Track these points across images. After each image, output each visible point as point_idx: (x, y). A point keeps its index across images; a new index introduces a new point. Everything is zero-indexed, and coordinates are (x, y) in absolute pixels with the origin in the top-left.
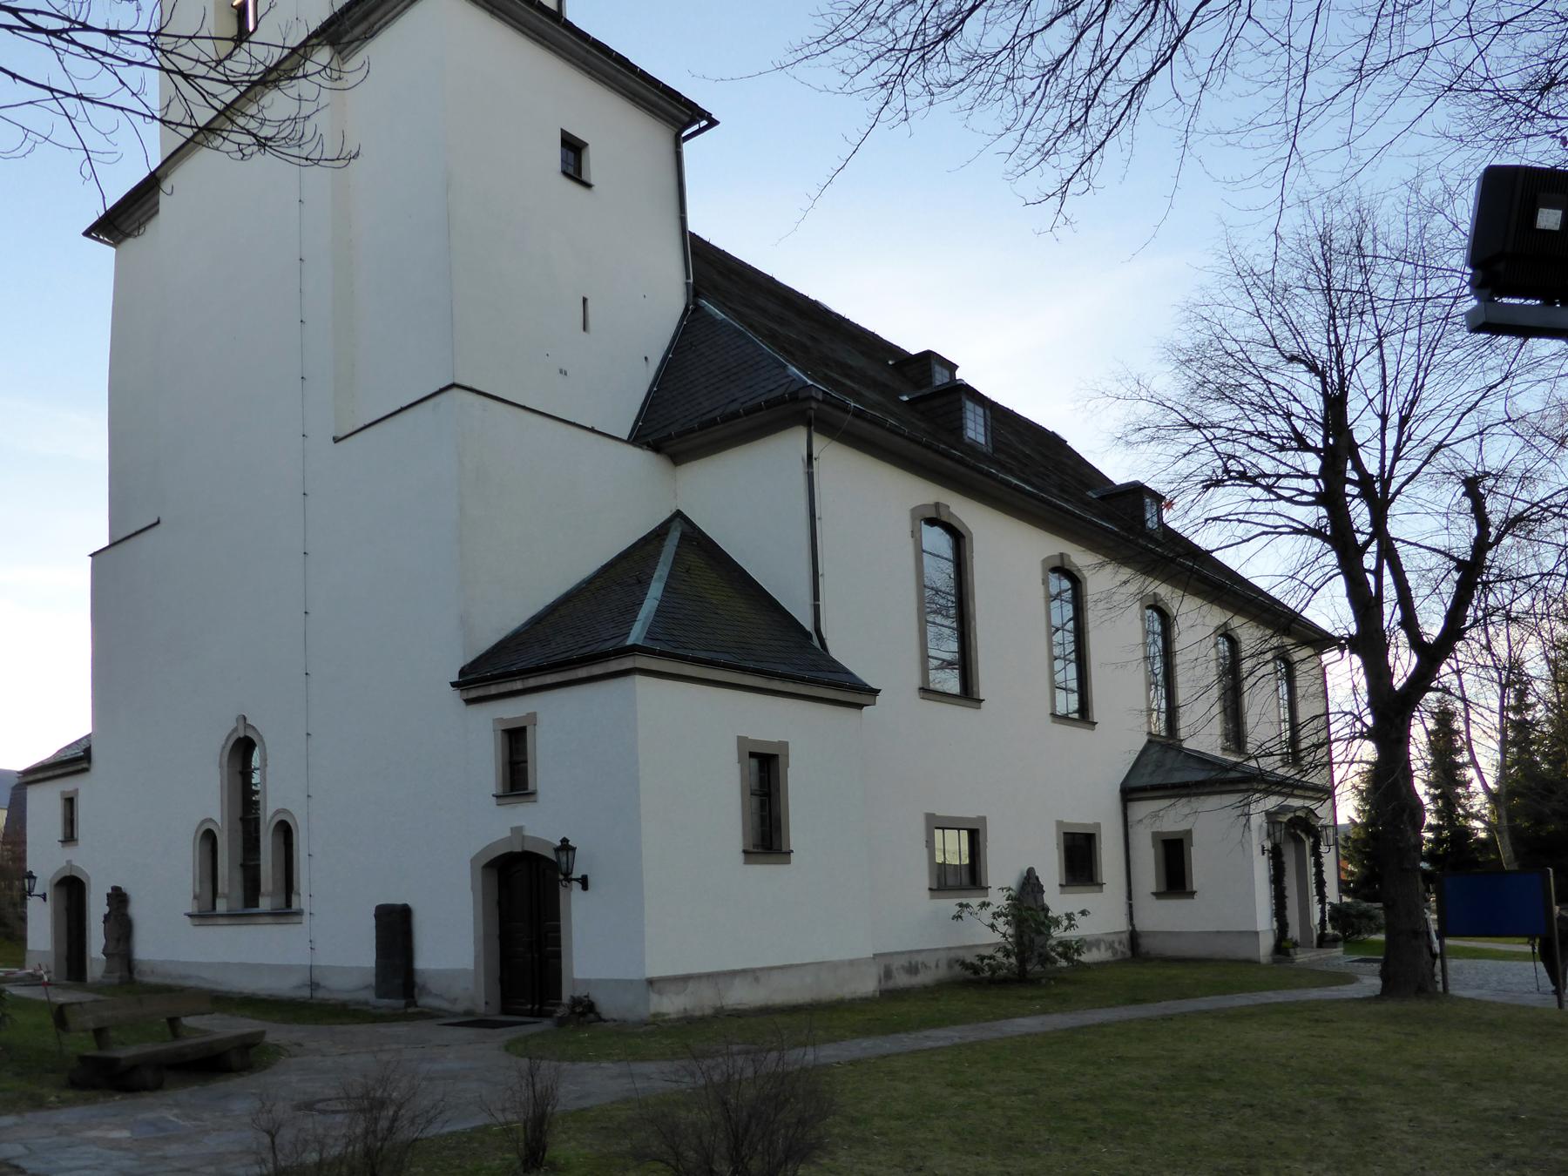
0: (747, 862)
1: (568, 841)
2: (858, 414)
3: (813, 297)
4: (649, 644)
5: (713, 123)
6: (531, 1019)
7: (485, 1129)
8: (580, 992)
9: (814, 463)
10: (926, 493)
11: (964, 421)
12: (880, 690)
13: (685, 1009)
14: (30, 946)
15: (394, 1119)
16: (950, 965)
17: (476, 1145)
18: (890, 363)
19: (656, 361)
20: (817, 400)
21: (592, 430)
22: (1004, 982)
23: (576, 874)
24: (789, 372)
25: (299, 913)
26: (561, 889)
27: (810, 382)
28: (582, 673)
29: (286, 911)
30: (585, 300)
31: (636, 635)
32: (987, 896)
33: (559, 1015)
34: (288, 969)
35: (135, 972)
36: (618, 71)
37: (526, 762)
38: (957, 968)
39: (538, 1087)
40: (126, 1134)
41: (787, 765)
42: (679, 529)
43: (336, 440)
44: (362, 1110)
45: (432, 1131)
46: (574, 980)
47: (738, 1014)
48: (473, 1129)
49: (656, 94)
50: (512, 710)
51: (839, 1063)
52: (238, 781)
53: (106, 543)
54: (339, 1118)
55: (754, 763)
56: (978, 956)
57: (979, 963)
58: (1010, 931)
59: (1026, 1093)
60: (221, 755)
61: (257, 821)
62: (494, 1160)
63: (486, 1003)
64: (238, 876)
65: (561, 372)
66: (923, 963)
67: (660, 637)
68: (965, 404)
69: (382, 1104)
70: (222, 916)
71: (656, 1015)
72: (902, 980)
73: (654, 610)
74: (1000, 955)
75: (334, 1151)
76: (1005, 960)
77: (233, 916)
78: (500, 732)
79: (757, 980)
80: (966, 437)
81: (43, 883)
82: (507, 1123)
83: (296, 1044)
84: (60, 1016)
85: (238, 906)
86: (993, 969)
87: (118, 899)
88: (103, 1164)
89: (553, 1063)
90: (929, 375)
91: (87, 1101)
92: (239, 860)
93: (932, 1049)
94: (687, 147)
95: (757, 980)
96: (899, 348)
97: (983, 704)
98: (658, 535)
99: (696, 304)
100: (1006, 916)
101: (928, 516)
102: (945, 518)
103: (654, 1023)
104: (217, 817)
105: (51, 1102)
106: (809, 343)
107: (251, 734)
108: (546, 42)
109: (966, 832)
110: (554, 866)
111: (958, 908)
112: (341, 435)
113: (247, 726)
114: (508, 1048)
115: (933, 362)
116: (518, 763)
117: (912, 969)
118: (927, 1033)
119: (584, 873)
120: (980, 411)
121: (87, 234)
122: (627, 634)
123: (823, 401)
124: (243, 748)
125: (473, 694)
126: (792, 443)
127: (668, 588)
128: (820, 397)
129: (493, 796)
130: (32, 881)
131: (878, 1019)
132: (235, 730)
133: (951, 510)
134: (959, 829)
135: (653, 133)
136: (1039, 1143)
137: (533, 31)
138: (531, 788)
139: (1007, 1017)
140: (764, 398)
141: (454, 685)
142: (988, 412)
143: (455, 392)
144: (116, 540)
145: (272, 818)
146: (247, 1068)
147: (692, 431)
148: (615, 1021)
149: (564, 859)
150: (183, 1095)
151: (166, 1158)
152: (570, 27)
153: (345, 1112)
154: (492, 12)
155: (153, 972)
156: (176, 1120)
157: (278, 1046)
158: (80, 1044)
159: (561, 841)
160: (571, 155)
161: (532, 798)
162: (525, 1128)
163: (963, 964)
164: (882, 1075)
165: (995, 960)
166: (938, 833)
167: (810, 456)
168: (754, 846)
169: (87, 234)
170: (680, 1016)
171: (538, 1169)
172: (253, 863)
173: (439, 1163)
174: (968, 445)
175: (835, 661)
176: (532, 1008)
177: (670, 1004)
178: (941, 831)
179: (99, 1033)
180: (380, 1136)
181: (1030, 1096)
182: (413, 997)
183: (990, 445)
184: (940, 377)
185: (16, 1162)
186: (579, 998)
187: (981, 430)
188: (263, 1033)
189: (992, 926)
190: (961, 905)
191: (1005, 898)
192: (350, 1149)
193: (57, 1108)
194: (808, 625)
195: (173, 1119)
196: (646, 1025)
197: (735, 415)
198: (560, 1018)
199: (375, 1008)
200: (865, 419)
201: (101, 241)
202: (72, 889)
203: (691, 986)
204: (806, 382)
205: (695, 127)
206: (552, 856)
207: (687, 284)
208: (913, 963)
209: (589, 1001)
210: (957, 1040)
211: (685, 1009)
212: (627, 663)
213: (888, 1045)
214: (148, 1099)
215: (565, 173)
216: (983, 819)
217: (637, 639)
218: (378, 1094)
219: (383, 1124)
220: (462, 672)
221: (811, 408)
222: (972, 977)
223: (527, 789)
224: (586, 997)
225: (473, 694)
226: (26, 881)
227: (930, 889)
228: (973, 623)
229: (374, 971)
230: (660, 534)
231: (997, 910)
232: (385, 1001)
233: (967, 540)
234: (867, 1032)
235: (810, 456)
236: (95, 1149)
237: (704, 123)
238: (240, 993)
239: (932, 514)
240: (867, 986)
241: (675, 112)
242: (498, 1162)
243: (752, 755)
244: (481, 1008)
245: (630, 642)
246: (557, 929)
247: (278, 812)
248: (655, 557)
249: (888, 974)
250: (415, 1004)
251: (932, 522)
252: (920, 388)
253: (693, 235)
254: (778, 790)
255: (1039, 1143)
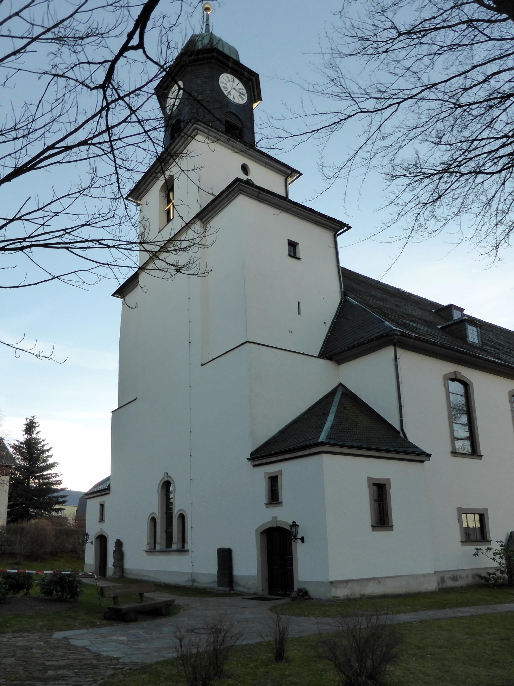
0: (373, 530)
1: (295, 522)
2: (416, 339)
3: (397, 287)
4: (328, 441)
5: (349, 228)
6: (281, 597)
7: (261, 642)
8: (302, 587)
9: (398, 360)
10: (450, 368)
11: (467, 334)
12: (431, 455)
13: (347, 595)
14: (86, 562)
15: (224, 637)
16: (474, 577)
17: (257, 649)
18: (433, 311)
19: (329, 324)
20: (397, 335)
21: (303, 354)
22: (502, 586)
23: (299, 536)
24: (385, 324)
25: (187, 551)
26: (293, 542)
27: (394, 328)
28: (300, 453)
29: (182, 550)
30: (299, 303)
31: (323, 437)
32: (490, 545)
33: (293, 596)
34: (184, 574)
35: (125, 573)
36: (310, 214)
37: (278, 490)
38: (477, 578)
39: (281, 627)
40: (125, 638)
41: (390, 488)
42: (341, 391)
43: (202, 365)
44: (213, 633)
45: (238, 643)
46: (299, 581)
47: (371, 597)
48: (255, 643)
49: (325, 220)
50: (272, 469)
51: (415, 621)
52: (165, 497)
53: (117, 407)
54: (203, 636)
55: (375, 488)
56: (487, 573)
57: (488, 576)
58: (503, 561)
59: (503, 639)
60: (158, 488)
61: (171, 514)
62: (264, 656)
63: (263, 590)
64: (164, 535)
65: (290, 332)
66: (460, 576)
67: (333, 437)
68: (467, 326)
69: (219, 631)
70: (158, 551)
71: (334, 597)
72: (450, 584)
73: (330, 426)
74: (498, 573)
75: (201, 650)
76: (501, 575)
77: (162, 552)
78: (267, 478)
79: (379, 582)
80: (468, 341)
81: (92, 537)
82: (268, 642)
83: (186, 605)
84: (102, 591)
85: (164, 547)
86: (496, 580)
87: (119, 544)
88: (117, 650)
89: (287, 617)
90: (451, 315)
91: (111, 625)
92: (165, 529)
93: (460, 617)
94: (338, 238)
95: (379, 582)
96: (437, 303)
97: (483, 457)
98: (332, 394)
99: (345, 299)
100: (500, 554)
101: (451, 377)
102: (459, 378)
103: (333, 601)
104: (157, 512)
105: (98, 625)
106: (395, 308)
107: (169, 479)
108: (281, 208)
109: (478, 515)
110: (289, 533)
111: (476, 551)
112: (204, 363)
113: (168, 476)
114: (270, 609)
115: (453, 309)
116: (275, 490)
117: (455, 579)
118: (460, 609)
119: (302, 536)
120: (475, 329)
121: (113, 295)
122: (319, 437)
123: (401, 335)
124: (167, 485)
125: (256, 463)
126: (388, 353)
127: (336, 416)
128: (399, 333)
129: (265, 504)
130: (88, 536)
131: (436, 602)
132: (164, 478)
133: (462, 374)
134: (474, 514)
135: (326, 235)
136: (506, 663)
137: (276, 205)
138: (280, 500)
139: (501, 603)
140: (375, 336)
141: (248, 459)
142: (479, 329)
143: (248, 344)
144: (121, 406)
145: (177, 512)
146: (168, 614)
147: (345, 351)
148: (316, 599)
149: (293, 529)
150: (145, 624)
151: (139, 648)
152: (291, 202)
153: (206, 633)
154: (260, 201)
155: (131, 573)
156: (143, 634)
157: (179, 605)
158: (108, 603)
159: (293, 522)
160: (292, 248)
161: (281, 505)
162: (276, 643)
163: (480, 577)
164: (435, 628)
165: (496, 575)
166: (464, 516)
167: (396, 358)
168: (377, 523)
169: (113, 295)
170: (345, 598)
171: (282, 661)
172: (170, 530)
173: (242, 656)
174: (469, 344)
175: (411, 443)
176: (281, 593)
177: (341, 593)
178: (465, 515)
179: (115, 598)
180: (219, 643)
181: (506, 641)
182: (232, 586)
183: (481, 343)
184: (457, 316)
185: (87, 647)
186: (301, 589)
187: (476, 337)
188: (174, 600)
189: (494, 559)
190: (477, 549)
191: (499, 546)
192: (208, 648)
193: (100, 627)
194: (398, 428)
195: (143, 634)
196: (330, 601)
197: (363, 343)
198: (293, 597)
199: (217, 591)
200: (419, 340)
201: (118, 297)
202: (102, 539)
203: (350, 585)
204: (393, 328)
205: (342, 230)
206: (289, 528)
207: (341, 291)
208: (455, 576)
209: (305, 590)
210: (474, 613)
211: (347, 595)
212: (319, 449)
213: (440, 614)
214: (132, 625)
215: (290, 255)
216: (486, 509)
217: (323, 439)
218: (219, 627)
219: (220, 639)
220: (252, 454)
221: (395, 339)
222: (485, 583)
223: (278, 501)
224: (304, 588)
225: (256, 463)
226: (86, 536)
227: (461, 542)
228: (475, 422)
229: (217, 576)
230: (332, 394)
231: (496, 551)
232: (221, 588)
233: (470, 386)
234: (430, 607)
235: (396, 358)
236: (115, 644)
237: (345, 228)
238: (164, 583)
239: (453, 376)
240: (432, 586)
241: (334, 226)
242: (265, 657)
243: (374, 484)
244: (260, 592)
245: (320, 440)
246: (291, 559)
247: (180, 510)
248: (331, 404)
249: (443, 580)
250: (233, 590)
251: (453, 380)
252: (448, 321)
253: (344, 269)
254: (386, 499)
255: (506, 663)
